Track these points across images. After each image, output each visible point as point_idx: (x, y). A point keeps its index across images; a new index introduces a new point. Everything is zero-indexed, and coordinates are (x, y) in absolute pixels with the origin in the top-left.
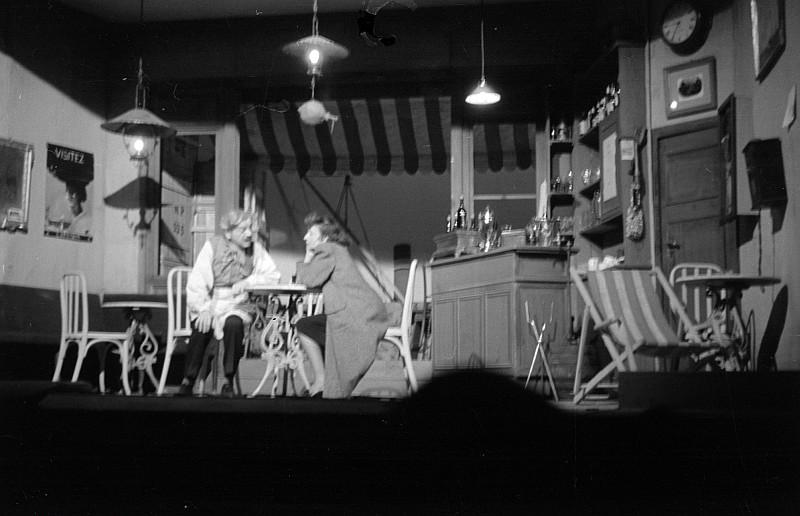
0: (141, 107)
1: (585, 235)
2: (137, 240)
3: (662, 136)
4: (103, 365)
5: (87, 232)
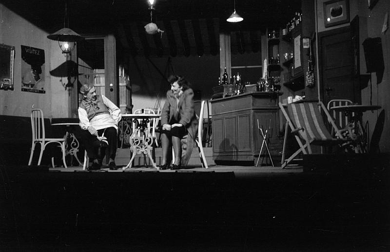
1: (285, 85)
2: (67, 92)
3: (322, 36)
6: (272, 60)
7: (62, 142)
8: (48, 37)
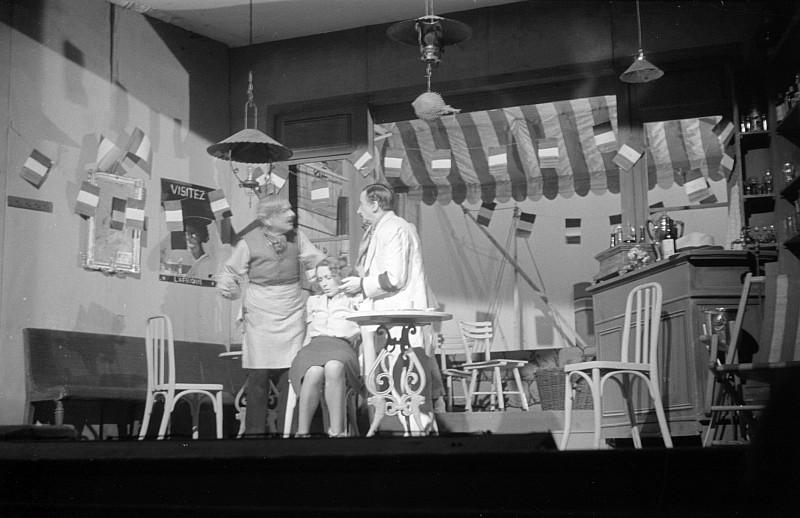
0: (251, 126)
4: (196, 420)
5: (210, 276)
6: (752, 186)
7: (214, 392)
8: (211, 151)
